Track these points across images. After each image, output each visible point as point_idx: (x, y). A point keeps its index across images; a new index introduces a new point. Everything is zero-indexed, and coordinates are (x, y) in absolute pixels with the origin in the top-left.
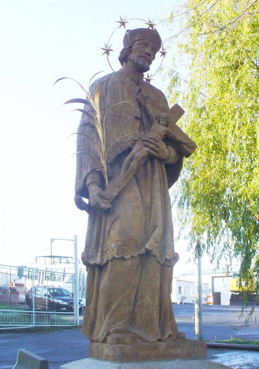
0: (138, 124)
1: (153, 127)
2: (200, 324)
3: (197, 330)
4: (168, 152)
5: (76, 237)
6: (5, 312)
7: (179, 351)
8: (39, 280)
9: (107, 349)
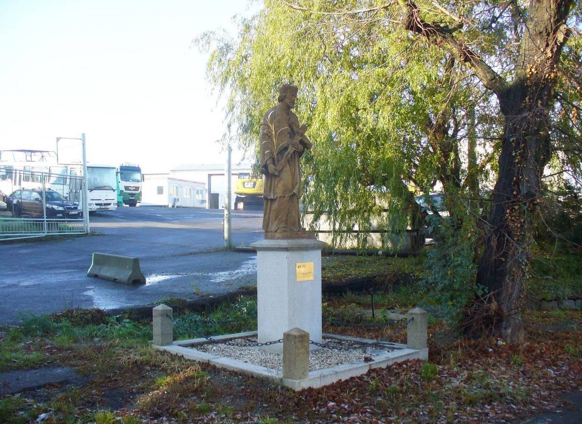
0: (289, 135)
1: (295, 137)
2: (229, 229)
3: (226, 235)
4: (301, 147)
5: (84, 135)
6: (8, 221)
7: (306, 235)
8: (15, 181)
9: (277, 235)
